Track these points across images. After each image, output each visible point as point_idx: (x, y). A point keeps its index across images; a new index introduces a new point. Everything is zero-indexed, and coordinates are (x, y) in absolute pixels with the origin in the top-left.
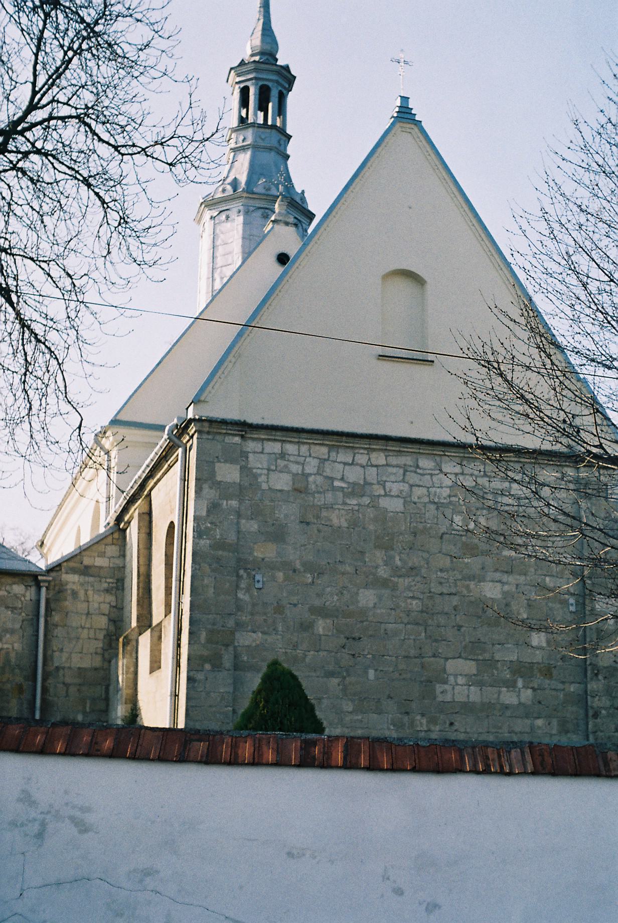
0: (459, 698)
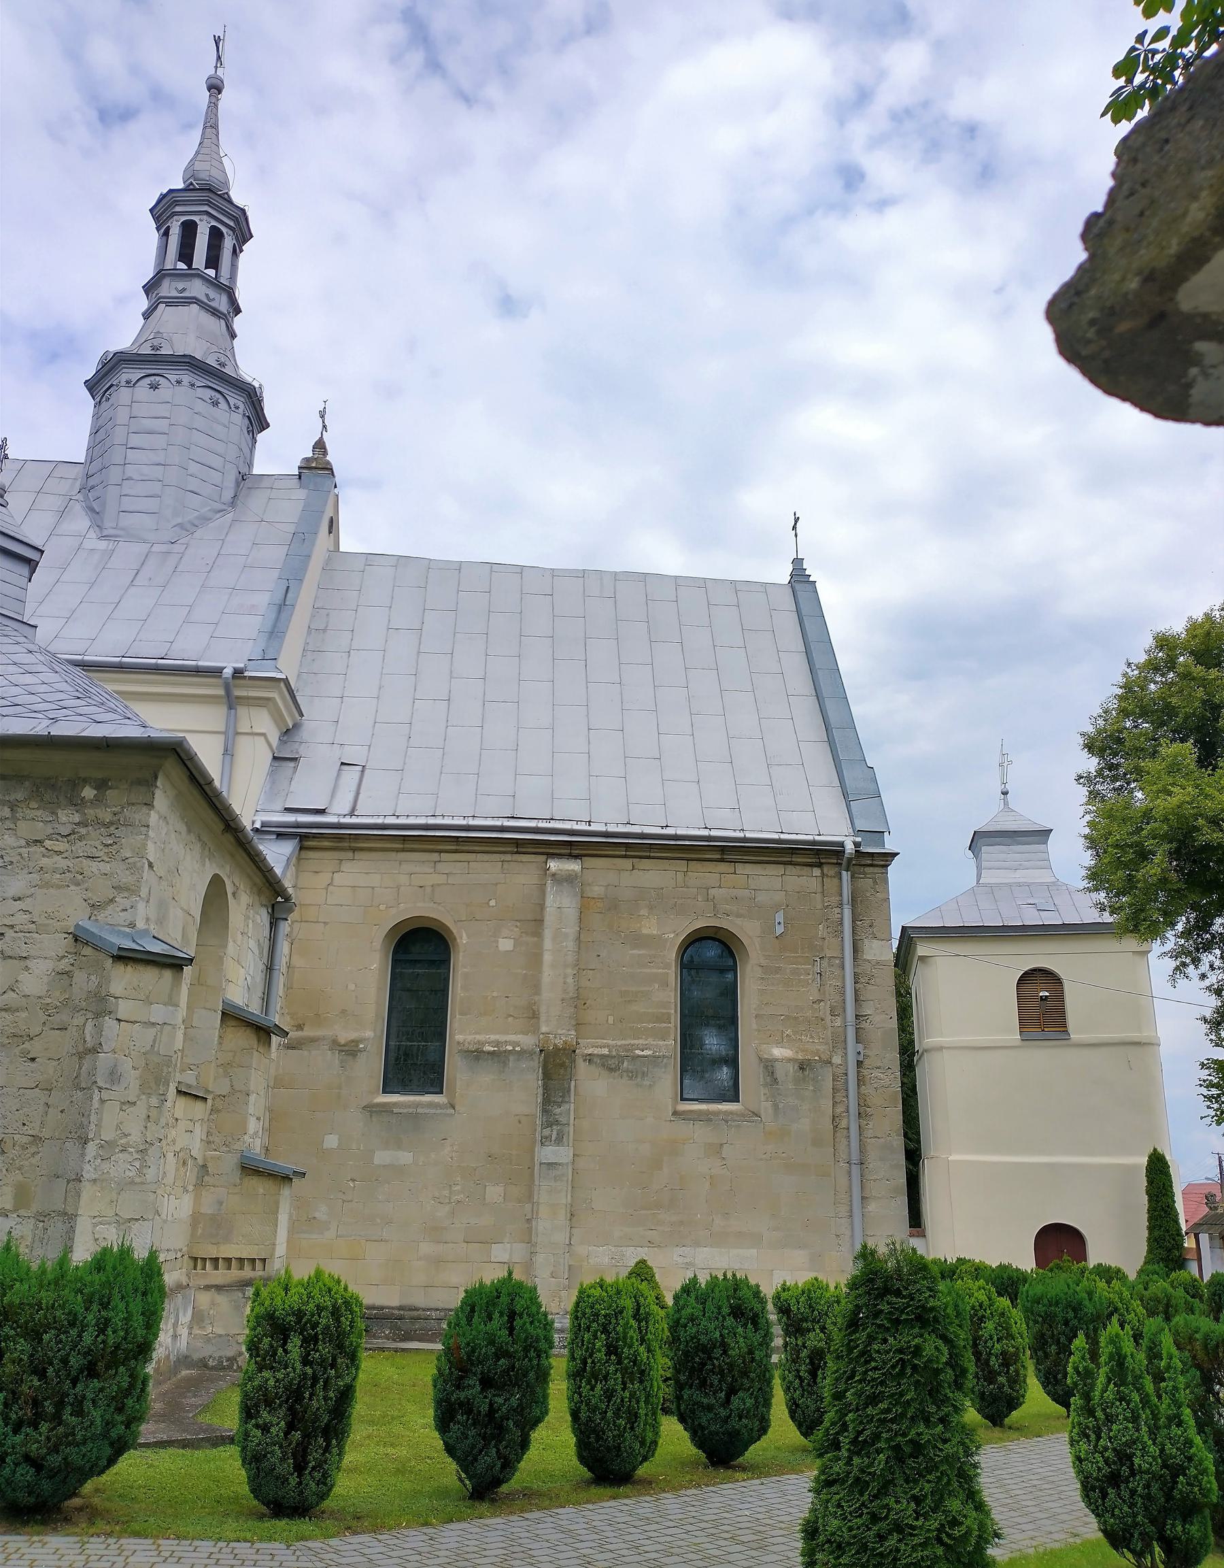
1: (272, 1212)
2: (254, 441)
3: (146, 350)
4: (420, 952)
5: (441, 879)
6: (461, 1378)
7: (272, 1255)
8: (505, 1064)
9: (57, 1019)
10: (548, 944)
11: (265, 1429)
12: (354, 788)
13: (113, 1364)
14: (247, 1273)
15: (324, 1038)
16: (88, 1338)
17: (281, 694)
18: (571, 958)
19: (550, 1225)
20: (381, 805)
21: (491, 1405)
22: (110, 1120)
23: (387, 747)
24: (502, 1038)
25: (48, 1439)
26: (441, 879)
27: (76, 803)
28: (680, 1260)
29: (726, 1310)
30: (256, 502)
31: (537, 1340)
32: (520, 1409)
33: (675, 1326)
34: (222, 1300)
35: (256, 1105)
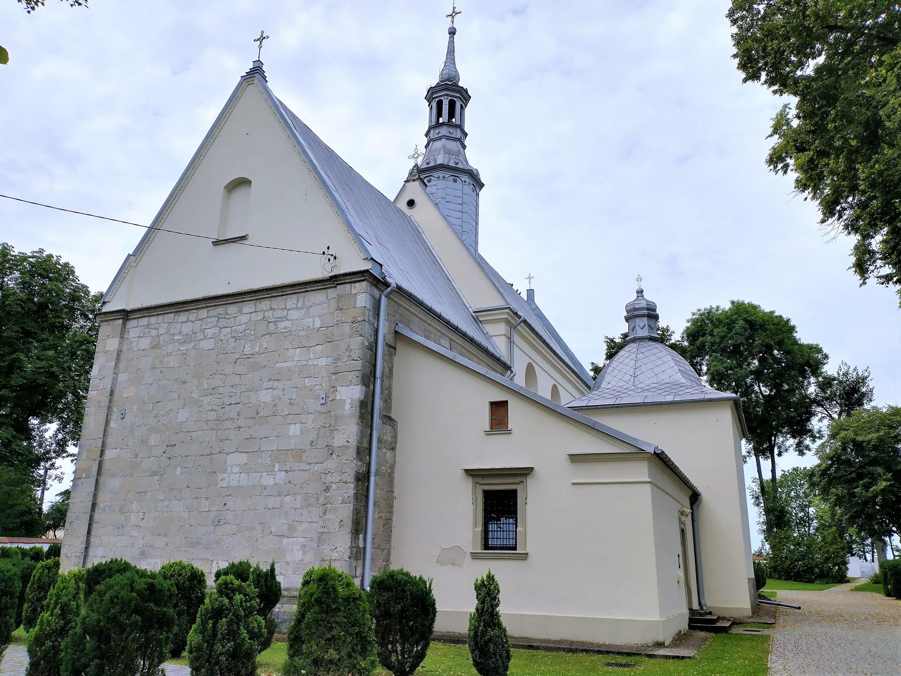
0: (233, 483)
2: (478, 195)
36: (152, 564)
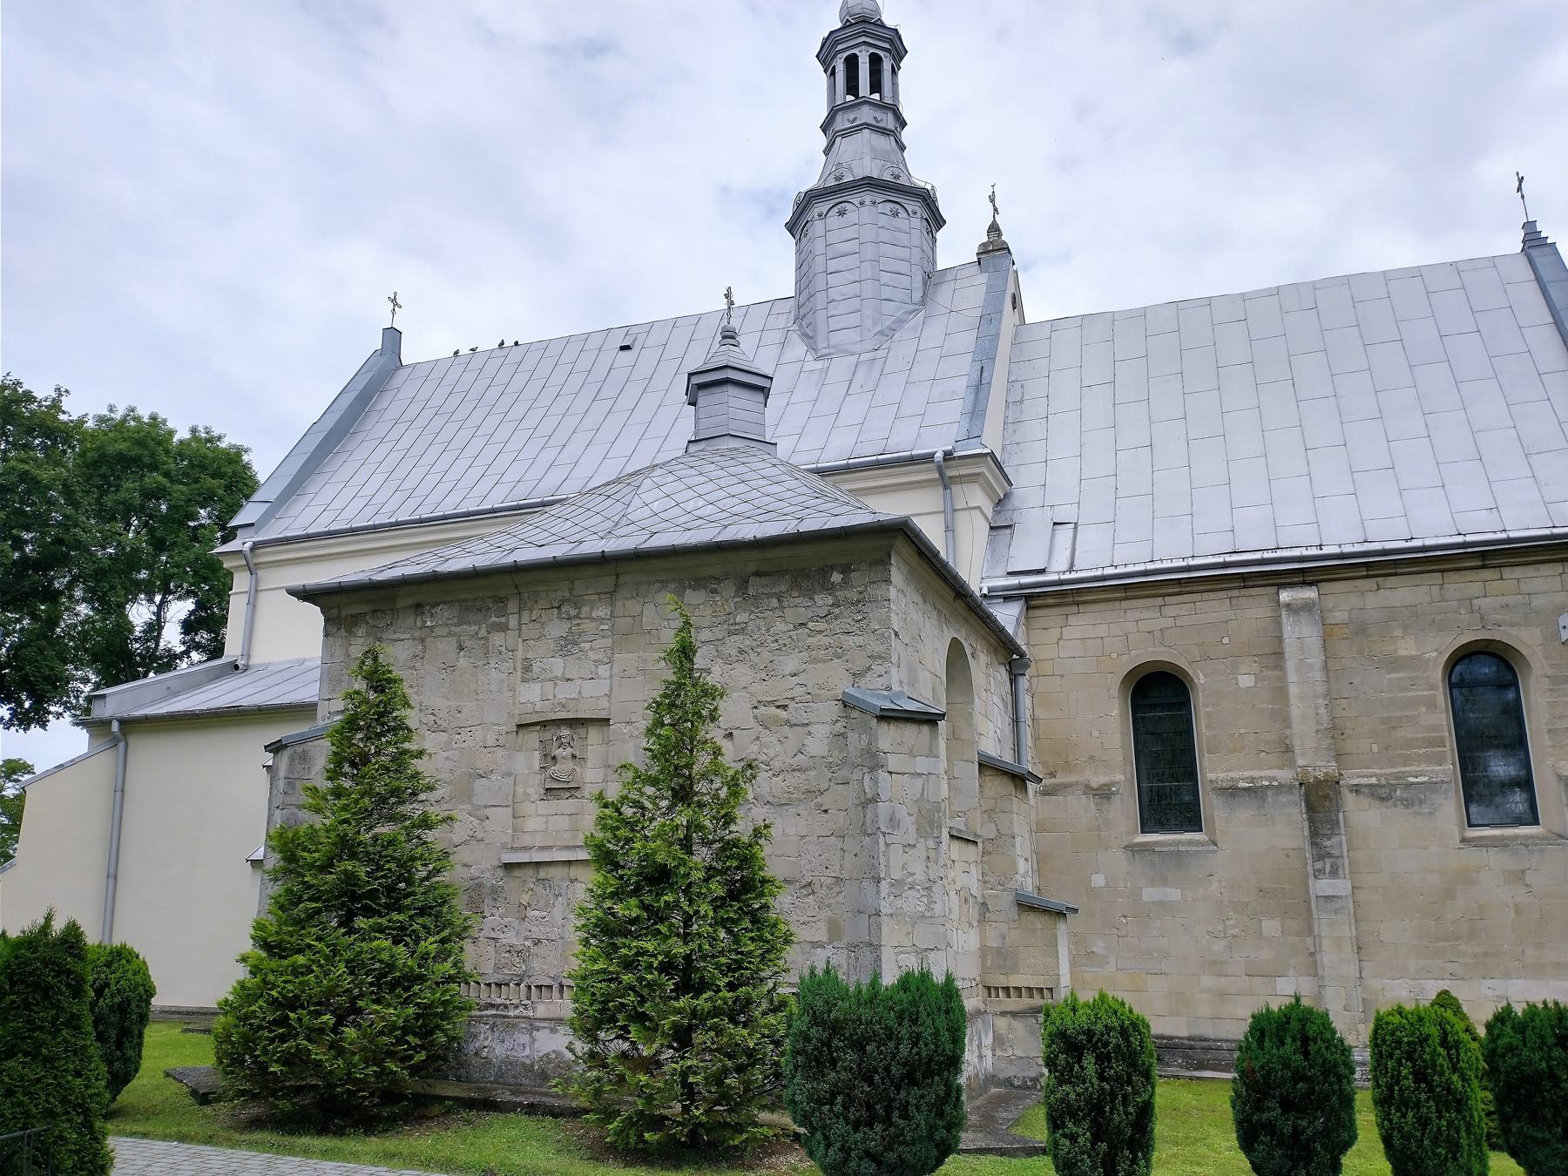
1: (1053, 945)
2: (934, 240)
3: (832, 182)
4: (1159, 697)
5: (1170, 622)
6: (1259, 1101)
7: (1058, 984)
8: (1264, 799)
9: (840, 775)
10: (1292, 676)
11: (1073, 1138)
12: (1069, 545)
13: (929, 1073)
14: (1037, 1001)
15: (1077, 784)
16: (904, 1050)
17: (989, 467)
18: (1320, 689)
19: (1336, 960)
20: (1097, 556)
21: (1295, 1127)
22: (896, 863)
23: (1099, 500)
24: (1257, 774)
25: (883, 1138)
26: (1170, 622)
27: (830, 589)
28: (1489, 993)
29: (1551, 1041)
30: (943, 296)
31: (1336, 1065)
32: (1326, 1132)
33: (1491, 1055)
34: (1017, 1024)
35: (1022, 846)
36: (85, 405)
